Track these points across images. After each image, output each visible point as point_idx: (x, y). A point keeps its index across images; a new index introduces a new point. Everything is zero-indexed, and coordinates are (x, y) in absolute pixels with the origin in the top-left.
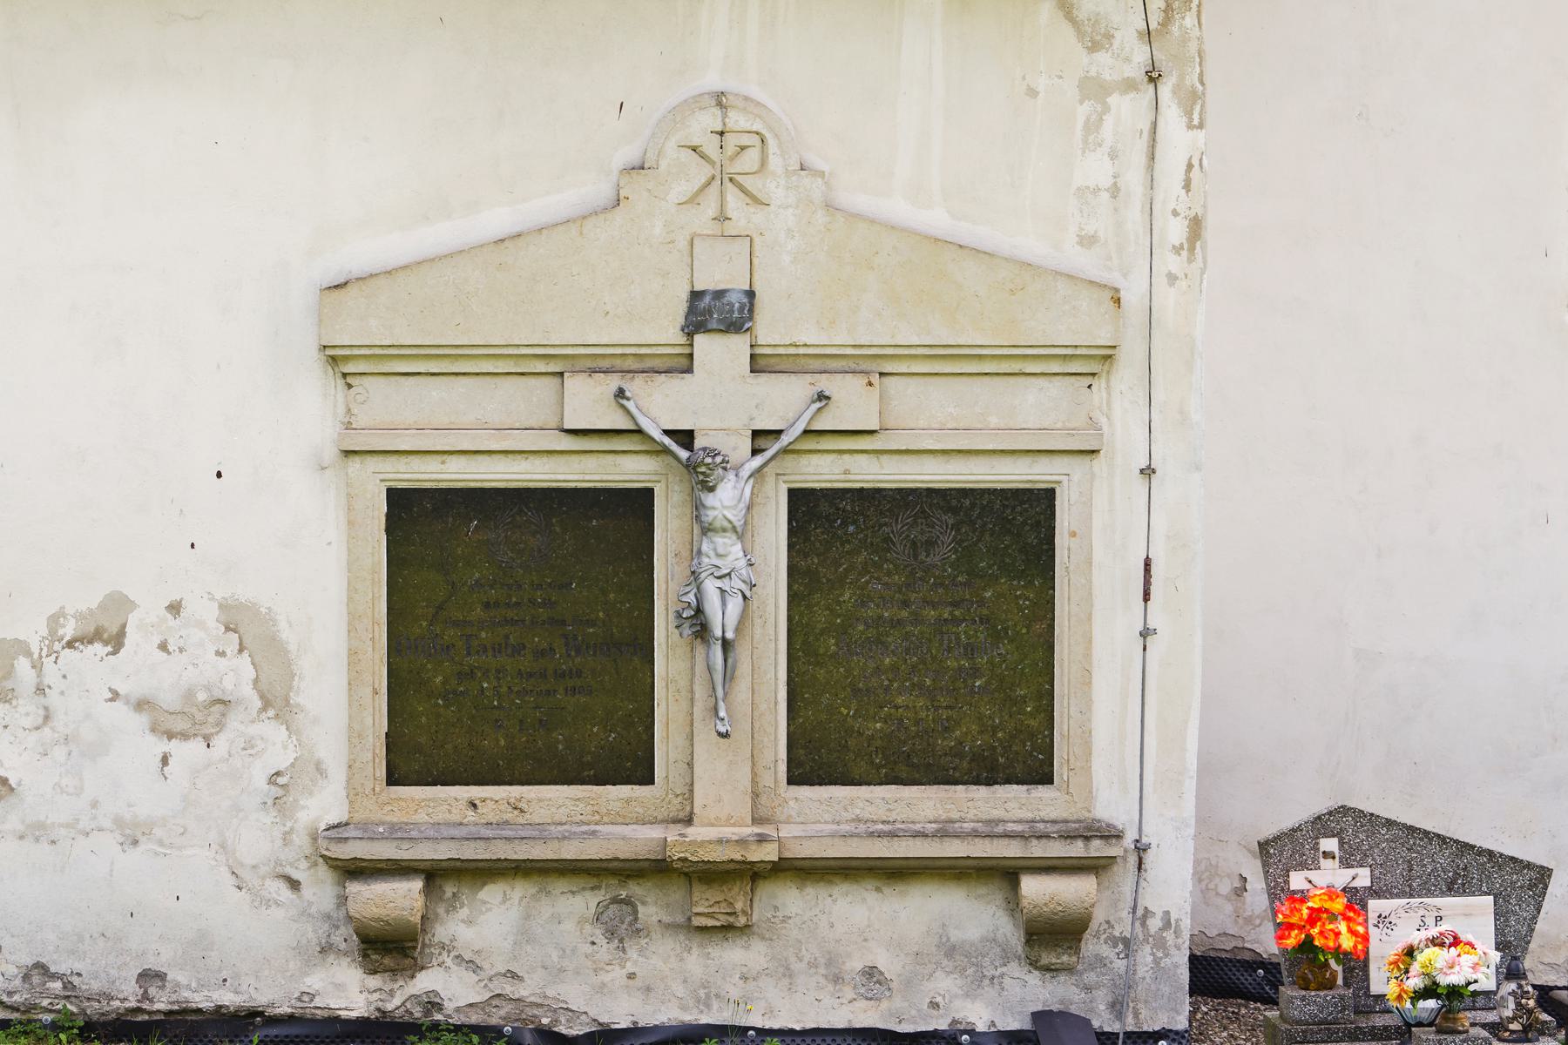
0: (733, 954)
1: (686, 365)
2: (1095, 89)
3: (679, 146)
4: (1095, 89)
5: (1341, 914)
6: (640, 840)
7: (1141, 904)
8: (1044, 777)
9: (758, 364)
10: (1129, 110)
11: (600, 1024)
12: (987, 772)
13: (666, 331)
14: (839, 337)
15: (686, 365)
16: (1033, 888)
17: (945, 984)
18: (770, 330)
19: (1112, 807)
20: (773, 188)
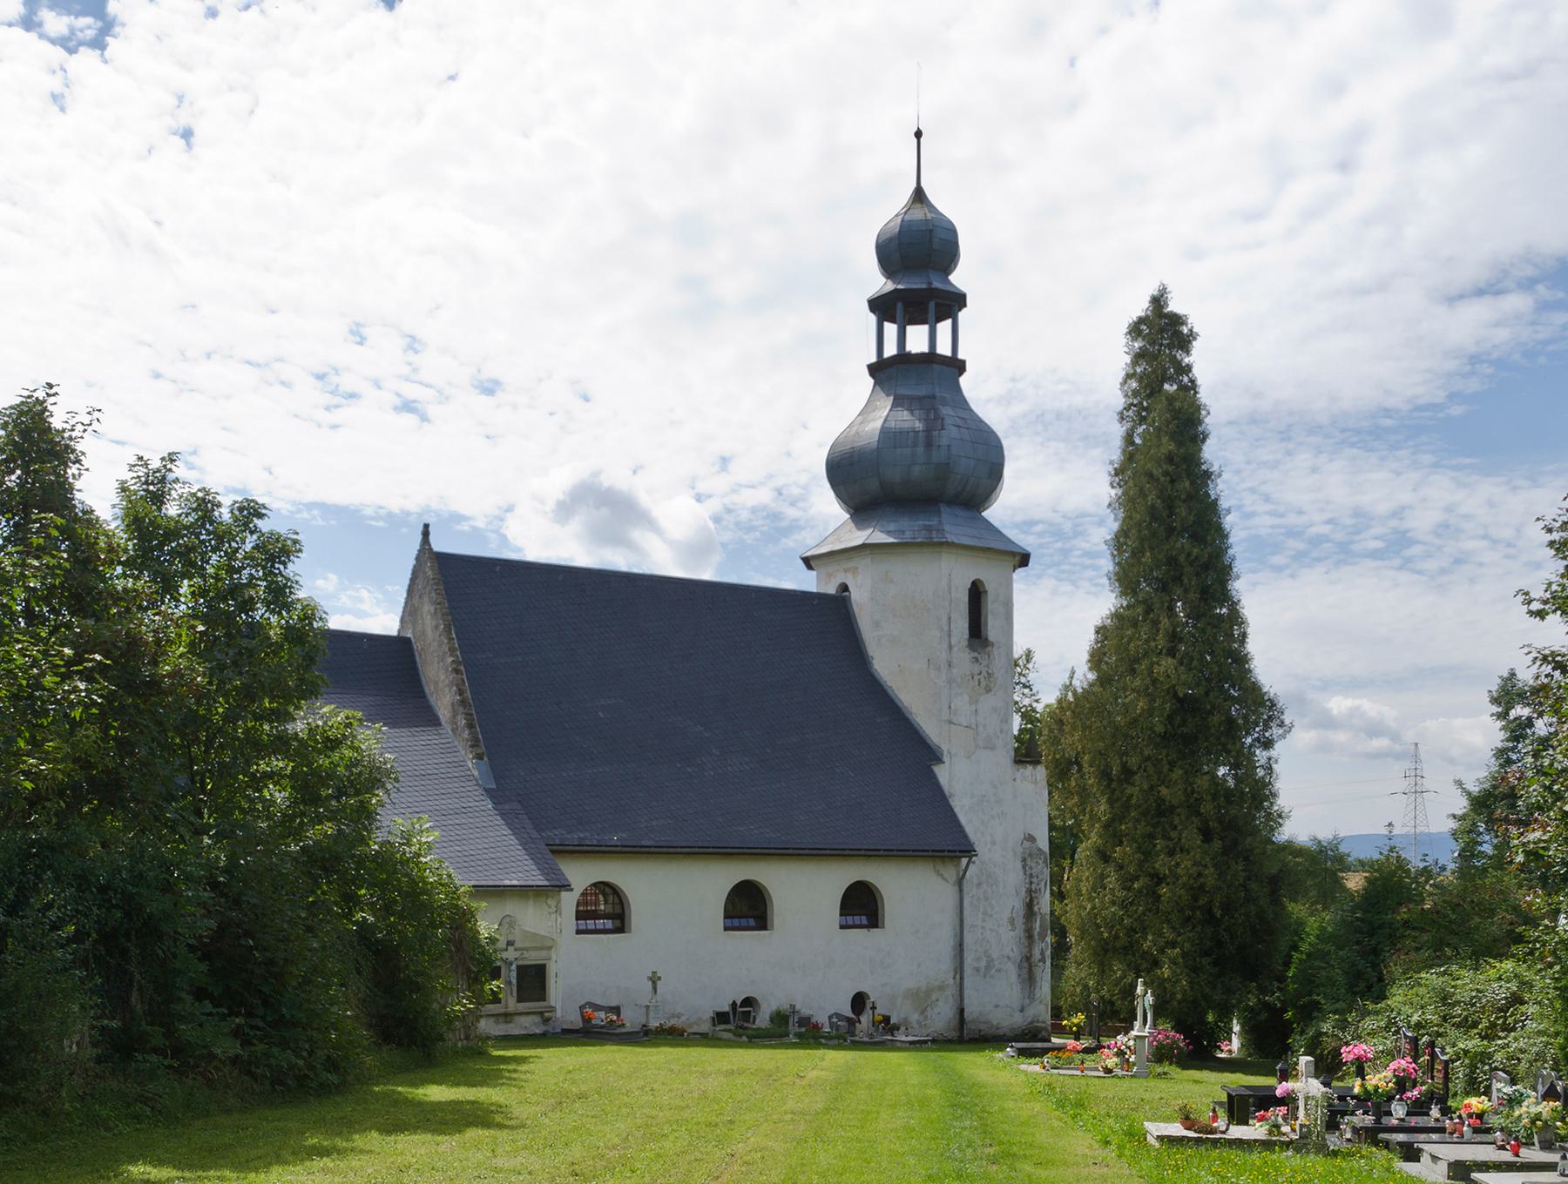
0: (511, 1025)
1: (507, 950)
2: (550, 913)
3: (426, 526)
4: (550, 913)
5: (848, 1033)
6: (502, 1011)
7: (705, 1027)
8: (545, 1000)
9: (516, 950)
10: (553, 916)
11: (1536, 265)
12: (539, 1000)
13: (505, 946)
14: (523, 946)
15: (507, 950)
16: (546, 1014)
17: (533, 1028)
18: (516, 945)
19: (553, 1004)
20: (516, 927)
